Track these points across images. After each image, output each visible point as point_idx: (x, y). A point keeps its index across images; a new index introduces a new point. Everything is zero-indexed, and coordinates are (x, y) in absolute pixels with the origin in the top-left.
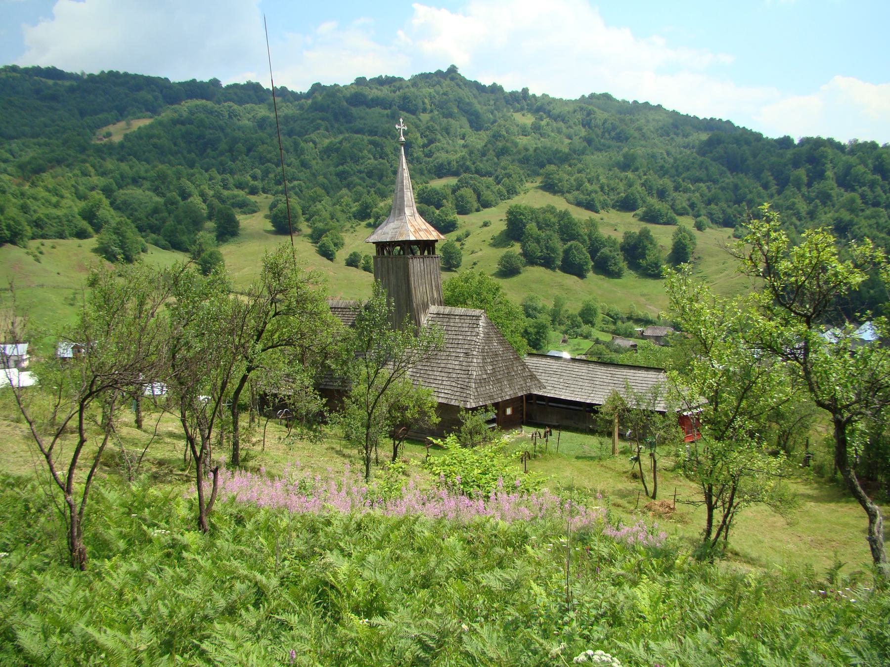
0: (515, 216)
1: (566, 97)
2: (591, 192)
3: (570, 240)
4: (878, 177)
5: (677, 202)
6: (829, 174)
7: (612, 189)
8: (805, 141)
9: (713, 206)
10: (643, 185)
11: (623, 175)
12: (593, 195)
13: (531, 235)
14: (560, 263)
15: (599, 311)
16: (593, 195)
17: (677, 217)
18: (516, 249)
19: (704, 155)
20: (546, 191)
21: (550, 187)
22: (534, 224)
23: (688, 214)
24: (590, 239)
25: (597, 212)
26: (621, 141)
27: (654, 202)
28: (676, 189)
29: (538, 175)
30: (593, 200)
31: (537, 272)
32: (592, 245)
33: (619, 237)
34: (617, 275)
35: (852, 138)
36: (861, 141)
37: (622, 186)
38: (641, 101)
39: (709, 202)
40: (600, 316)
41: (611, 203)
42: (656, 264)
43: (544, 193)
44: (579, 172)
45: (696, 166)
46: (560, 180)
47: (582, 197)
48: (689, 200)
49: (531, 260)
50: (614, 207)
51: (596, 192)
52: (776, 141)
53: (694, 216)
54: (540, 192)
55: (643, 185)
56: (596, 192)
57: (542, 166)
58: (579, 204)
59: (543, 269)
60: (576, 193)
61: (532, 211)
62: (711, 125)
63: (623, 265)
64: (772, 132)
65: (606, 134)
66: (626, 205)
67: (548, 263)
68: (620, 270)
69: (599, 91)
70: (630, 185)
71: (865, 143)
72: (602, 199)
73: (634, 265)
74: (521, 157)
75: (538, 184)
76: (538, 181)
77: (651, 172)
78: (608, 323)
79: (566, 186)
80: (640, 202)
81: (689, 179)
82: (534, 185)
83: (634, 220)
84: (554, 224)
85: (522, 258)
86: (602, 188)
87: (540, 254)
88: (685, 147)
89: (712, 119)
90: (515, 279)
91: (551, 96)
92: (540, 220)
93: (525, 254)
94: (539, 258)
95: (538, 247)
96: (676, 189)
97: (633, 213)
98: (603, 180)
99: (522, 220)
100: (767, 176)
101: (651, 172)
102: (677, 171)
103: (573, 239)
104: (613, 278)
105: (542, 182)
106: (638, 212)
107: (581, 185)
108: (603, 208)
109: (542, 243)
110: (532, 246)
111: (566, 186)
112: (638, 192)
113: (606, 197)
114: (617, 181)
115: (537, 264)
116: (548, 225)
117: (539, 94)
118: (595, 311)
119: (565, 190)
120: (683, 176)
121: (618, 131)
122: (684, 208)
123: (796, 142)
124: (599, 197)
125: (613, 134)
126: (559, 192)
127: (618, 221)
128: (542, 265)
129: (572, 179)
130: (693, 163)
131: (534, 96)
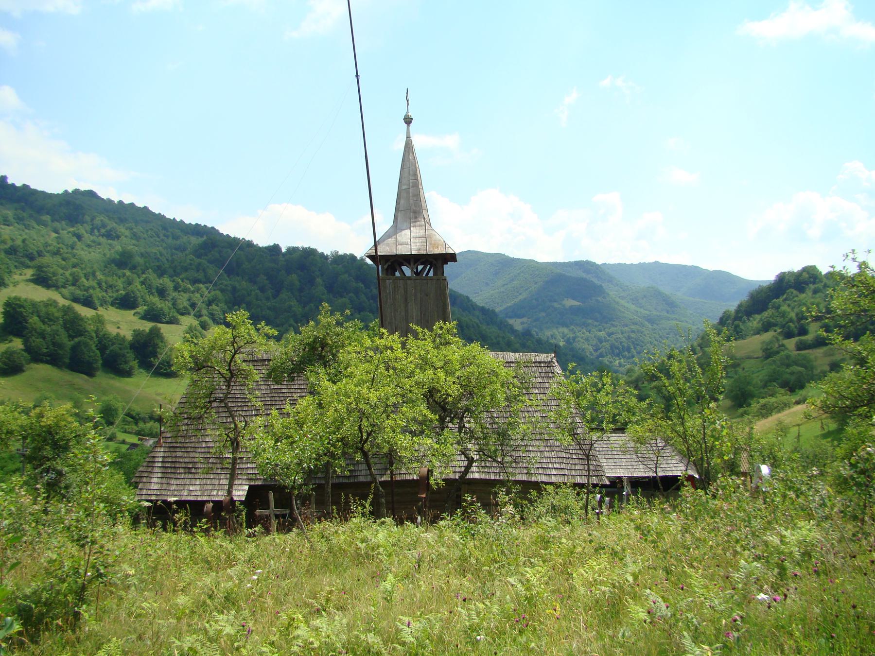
0: (14, 309)
1: (49, 191)
2: (89, 288)
3: (76, 337)
4: (361, 285)
5: (179, 301)
6: (319, 280)
7: (111, 286)
8: (292, 250)
9: (214, 307)
10: (143, 283)
11: (120, 272)
12: (91, 291)
13: (35, 330)
14: (67, 361)
15: (120, 411)
16: (91, 291)
17: (180, 317)
18: (17, 344)
19: (199, 257)
20: (38, 284)
21: (42, 280)
22: (36, 318)
23: (189, 314)
24: (97, 337)
25: (95, 309)
26: (113, 239)
27: (155, 300)
28: (176, 288)
29: (28, 267)
30: (91, 296)
31: (43, 370)
32: (100, 342)
33: (129, 335)
34: (128, 374)
35: (333, 250)
36: (341, 253)
37: (120, 283)
38: (126, 202)
39: (209, 303)
40: (121, 416)
41: (110, 300)
42: (168, 362)
43: (37, 286)
44: (74, 266)
45: (193, 267)
46: (54, 274)
47: (79, 293)
48: (189, 300)
49: (36, 357)
50: (113, 304)
51: (94, 288)
52: (266, 248)
53: (195, 315)
54: (32, 285)
55: (143, 283)
56: (94, 288)
57: (32, 259)
58: (76, 300)
59: (49, 367)
60: (72, 288)
61: (34, 304)
62: (198, 230)
63: (135, 364)
64: (262, 241)
65: (96, 231)
66: (126, 303)
67: (54, 360)
68: (131, 368)
69: (83, 188)
70: (130, 283)
71: (345, 255)
72: (100, 295)
73: (146, 365)
74: (7, 247)
75: (28, 277)
76: (29, 273)
77: (150, 270)
78: (129, 423)
79: (61, 280)
80: (140, 300)
81: (188, 279)
82: (23, 277)
83: (136, 319)
84: (57, 318)
85: (26, 354)
86: (100, 284)
87: (45, 351)
88: (176, 249)
89: (197, 224)
90: (17, 378)
91: (32, 187)
92: (42, 314)
93: (28, 349)
94: (44, 355)
95: (43, 343)
96: (176, 288)
97: (133, 312)
98: (100, 276)
99: (21, 313)
100: (262, 279)
101: (150, 270)
102: (175, 271)
103: (81, 335)
104: (123, 377)
105: (33, 275)
106: (138, 310)
107: (77, 281)
108: (102, 305)
109: (48, 338)
110: (36, 341)
111: (61, 280)
112: (138, 290)
113: (104, 294)
114: (115, 278)
115: (42, 361)
116: (51, 320)
117: (19, 184)
118: (116, 410)
119: (60, 284)
120: (183, 276)
121: (109, 228)
122: (185, 308)
123: (284, 250)
124: (97, 294)
125: (103, 231)
126: (53, 286)
127: (119, 319)
128: (47, 362)
129: (67, 273)
130: (191, 264)
131: (13, 185)
